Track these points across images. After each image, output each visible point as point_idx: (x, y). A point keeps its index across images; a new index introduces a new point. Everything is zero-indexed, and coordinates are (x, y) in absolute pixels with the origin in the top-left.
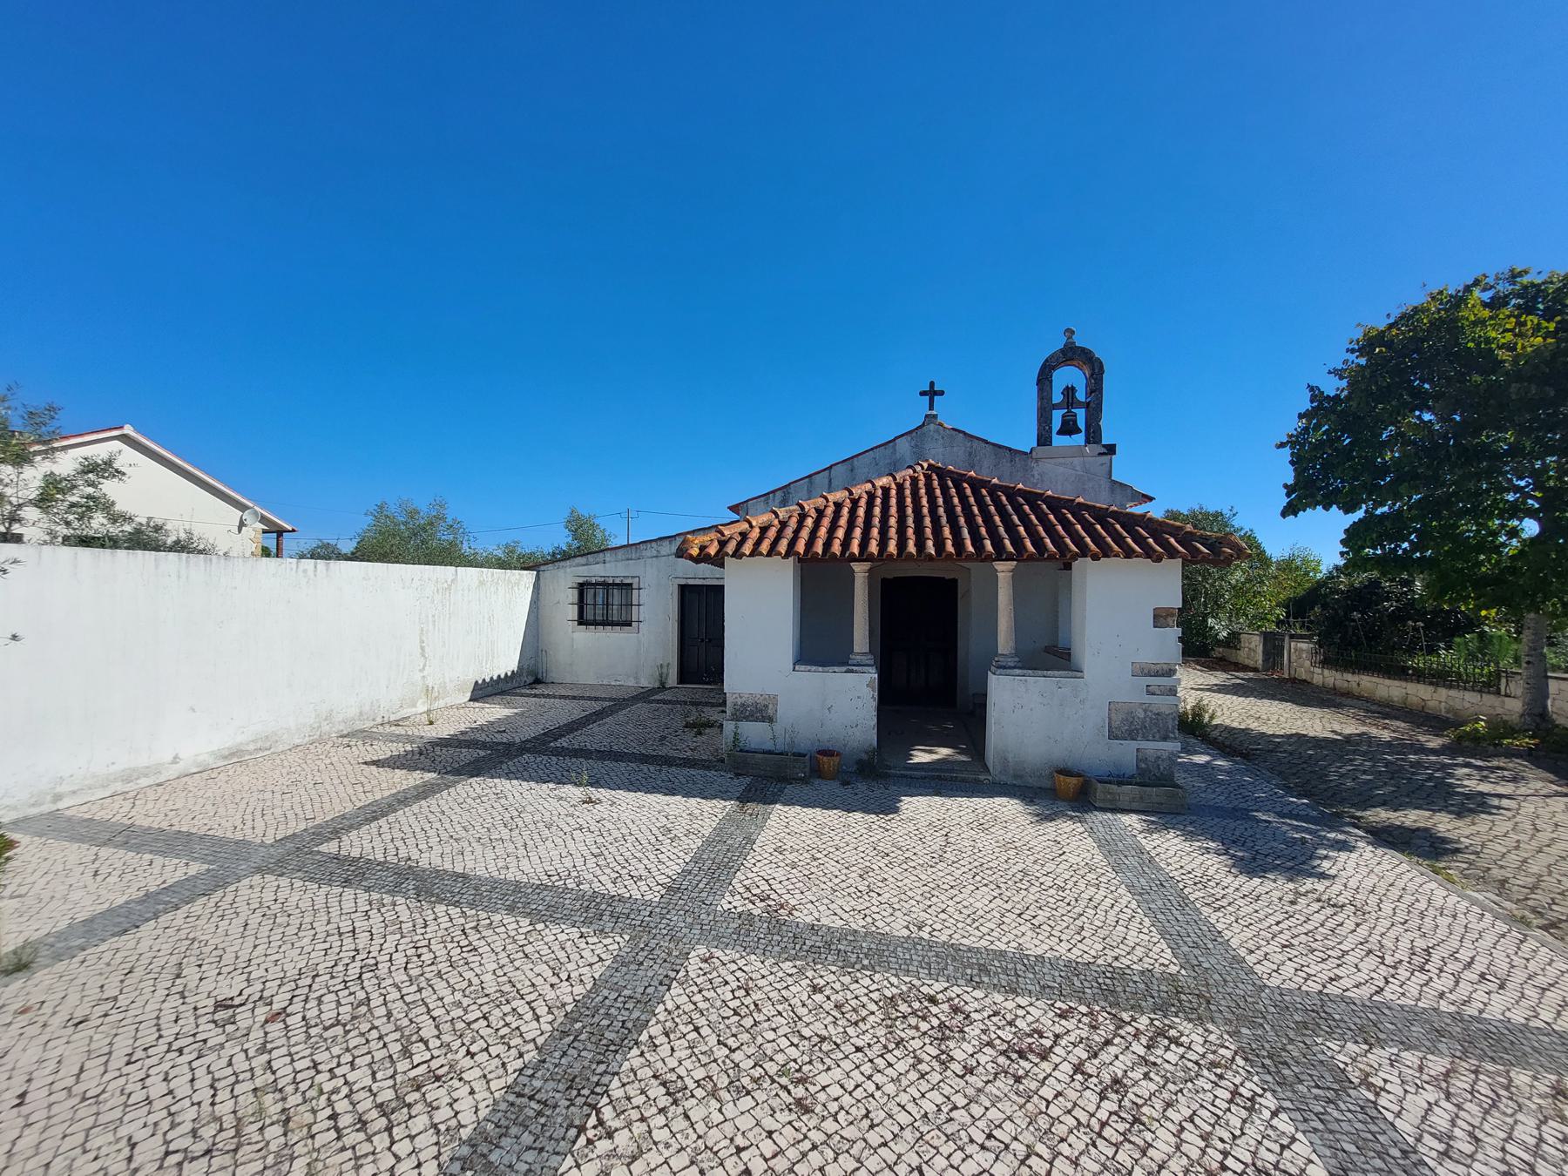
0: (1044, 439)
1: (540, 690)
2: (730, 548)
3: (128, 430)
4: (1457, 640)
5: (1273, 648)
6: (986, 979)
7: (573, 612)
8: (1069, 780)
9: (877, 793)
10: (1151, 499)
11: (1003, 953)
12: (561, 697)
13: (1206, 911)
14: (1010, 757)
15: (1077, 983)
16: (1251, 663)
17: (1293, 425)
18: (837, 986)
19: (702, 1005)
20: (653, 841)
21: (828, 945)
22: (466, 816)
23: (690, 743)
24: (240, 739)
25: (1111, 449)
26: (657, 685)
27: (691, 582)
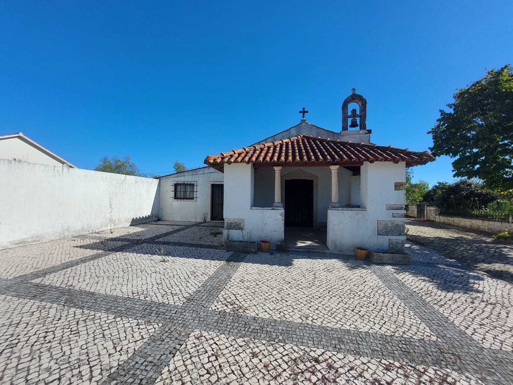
0: (345, 128)
1: (160, 222)
2: (226, 160)
3: (21, 134)
4: (489, 204)
5: (421, 211)
6: (343, 347)
7: (172, 194)
8: (362, 251)
9: (284, 257)
10: (428, 133)
11: (348, 331)
12: (167, 225)
13: (436, 307)
14: (338, 243)
15: (389, 348)
16: (413, 215)
17: (433, 124)
18: (266, 353)
19: (190, 367)
20: (186, 277)
21: (262, 328)
22: (108, 267)
23: (211, 240)
24: (24, 236)
25: (370, 132)
26: (203, 221)
27: (216, 183)
